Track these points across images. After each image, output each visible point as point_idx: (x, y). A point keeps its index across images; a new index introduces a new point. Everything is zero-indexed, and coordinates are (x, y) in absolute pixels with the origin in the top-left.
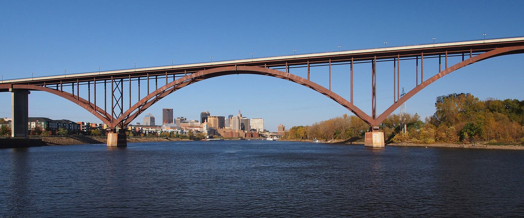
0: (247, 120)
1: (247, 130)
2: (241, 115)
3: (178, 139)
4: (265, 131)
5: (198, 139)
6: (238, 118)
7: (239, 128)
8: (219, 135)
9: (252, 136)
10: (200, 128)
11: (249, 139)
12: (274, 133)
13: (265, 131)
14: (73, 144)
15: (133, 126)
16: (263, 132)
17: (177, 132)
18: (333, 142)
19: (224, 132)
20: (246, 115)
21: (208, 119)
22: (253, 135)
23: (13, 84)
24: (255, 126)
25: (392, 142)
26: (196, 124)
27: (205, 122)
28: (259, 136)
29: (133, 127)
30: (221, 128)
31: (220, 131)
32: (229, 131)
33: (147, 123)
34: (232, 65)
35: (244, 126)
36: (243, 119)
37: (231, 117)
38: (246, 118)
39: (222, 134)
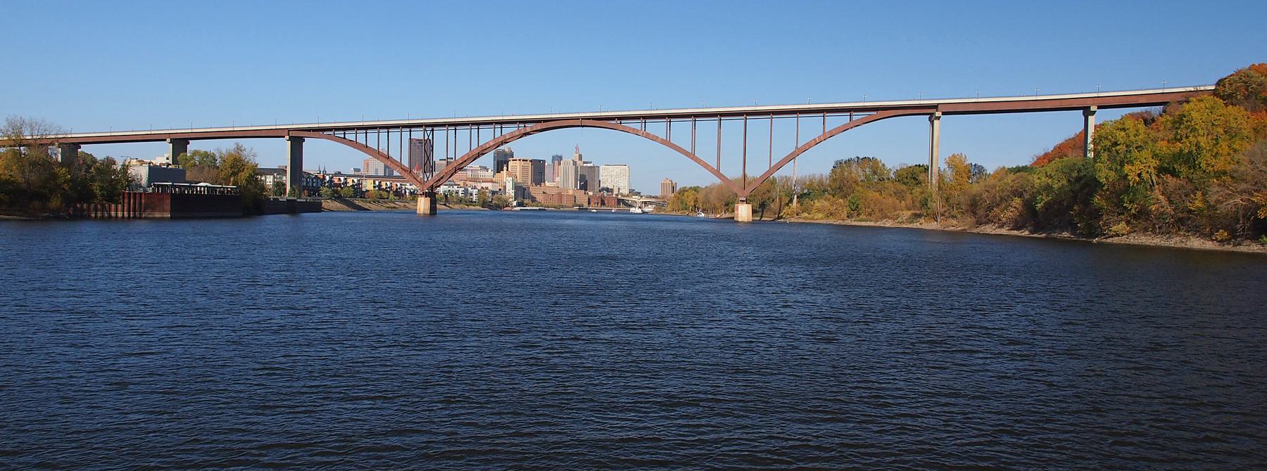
0: (594, 167)
1: (593, 190)
2: (580, 158)
3: (461, 206)
4: (632, 192)
5: (498, 207)
6: (575, 163)
7: (576, 186)
8: (534, 200)
9: (603, 203)
10: (495, 184)
11: (594, 208)
12: (651, 197)
13: (632, 192)
14: (351, 211)
15: (343, 175)
16: (628, 196)
17: (457, 193)
18: (724, 216)
19: (544, 192)
20: (591, 158)
21: (511, 163)
22: (606, 202)
23: (289, 130)
24: (610, 181)
25: (782, 218)
26: (482, 173)
27: (505, 171)
28: (619, 204)
29: (342, 178)
30: (536, 185)
31: (535, 191)
32: (555, 192)
33: (377, 170)
34: (577, 119)
35: (585, 180)
36: (585, 165)
37: (558, 159)
38: (591, 163)
39: (539, 198)
